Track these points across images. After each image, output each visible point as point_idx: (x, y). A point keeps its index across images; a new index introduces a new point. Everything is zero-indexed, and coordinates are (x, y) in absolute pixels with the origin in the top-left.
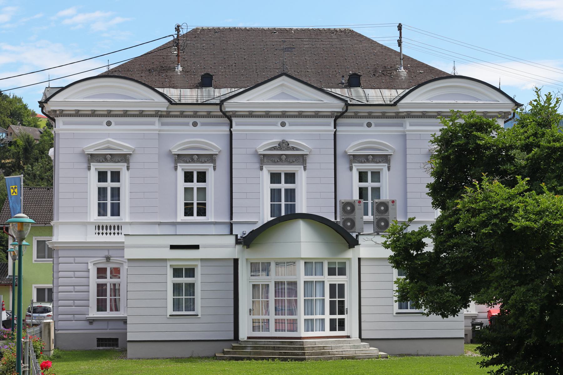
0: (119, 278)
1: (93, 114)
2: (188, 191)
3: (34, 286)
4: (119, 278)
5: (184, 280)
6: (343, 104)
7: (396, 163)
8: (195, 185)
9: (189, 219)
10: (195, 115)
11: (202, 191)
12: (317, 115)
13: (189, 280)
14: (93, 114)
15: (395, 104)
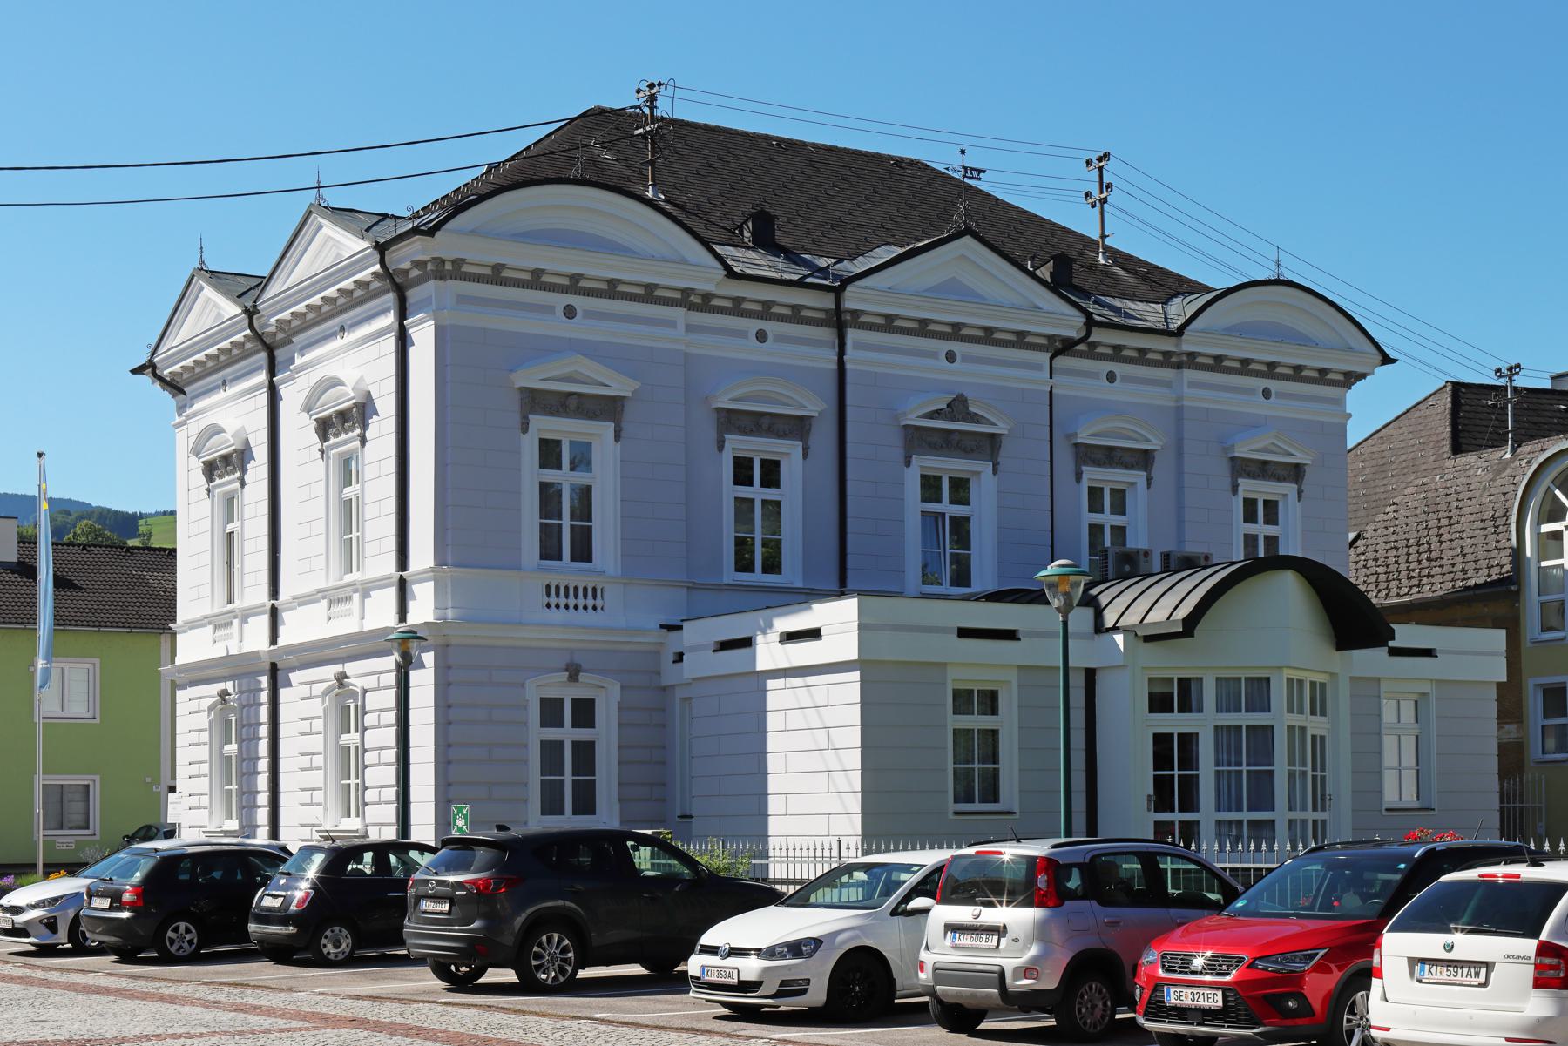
0: (1150, 680)
1: (923, 328)
2: (744, 505)
3: (97, 778)
4: (1150, 680)
5: (977, 722)
6: (1080, 319)
7: (1161, 468)
8: (757, 492)
9: (745, 577)
10: (766, 311)
11: (773, 509)
12: (1020, 340)
13: (987, 722)
14: (923, 328)
15: (1180, 331)
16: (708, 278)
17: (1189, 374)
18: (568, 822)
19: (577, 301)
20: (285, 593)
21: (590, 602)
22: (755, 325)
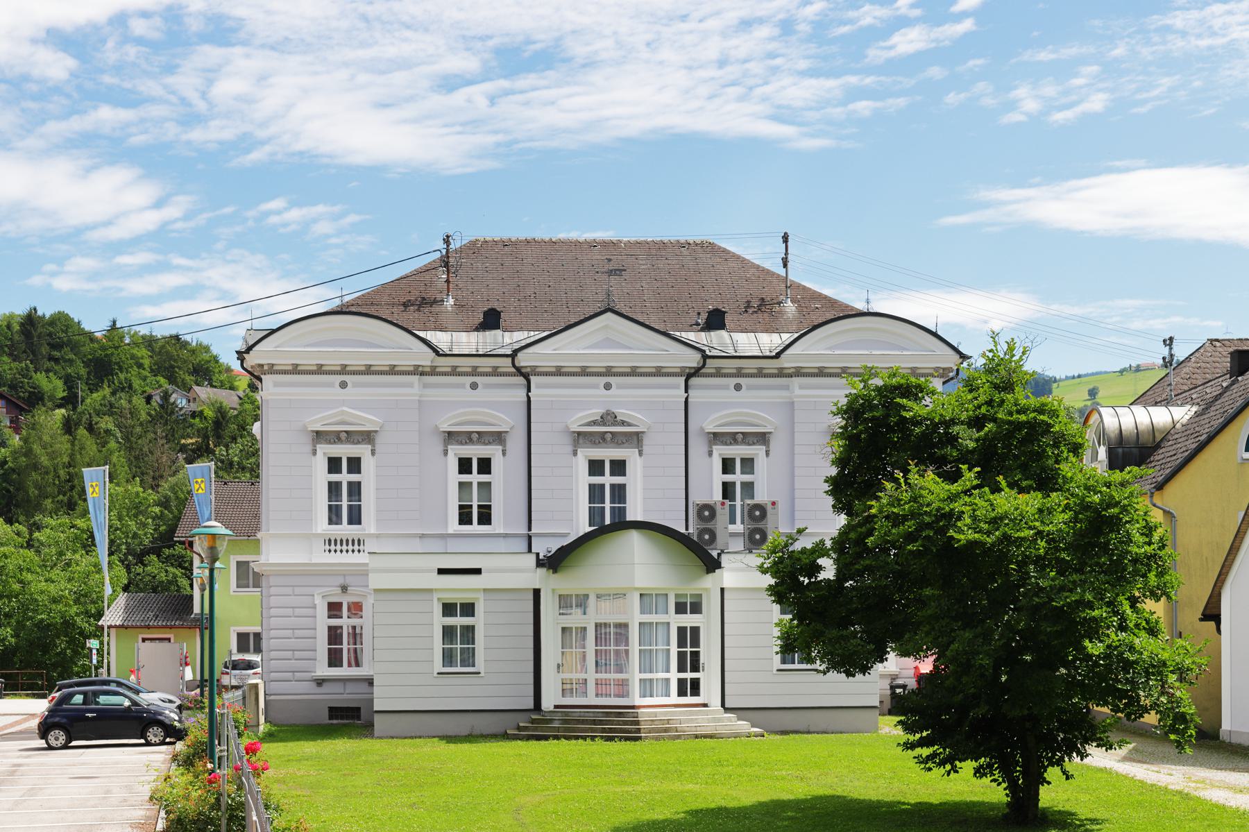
1: (320, 370)
5: (458, 621)
6: (698, 356)
8: (475, 478)
9: (466, 529)
10: (474, 372)
11: (485, 487)
13: (467, 621)
14: (320, 370)
15: (778, 356)
16: (425, 358)
17: (796, 381)
18: (344, 671)
19: (611, 380)
20: (533, 531)
21: (356, 547)
22: (603, 380)
